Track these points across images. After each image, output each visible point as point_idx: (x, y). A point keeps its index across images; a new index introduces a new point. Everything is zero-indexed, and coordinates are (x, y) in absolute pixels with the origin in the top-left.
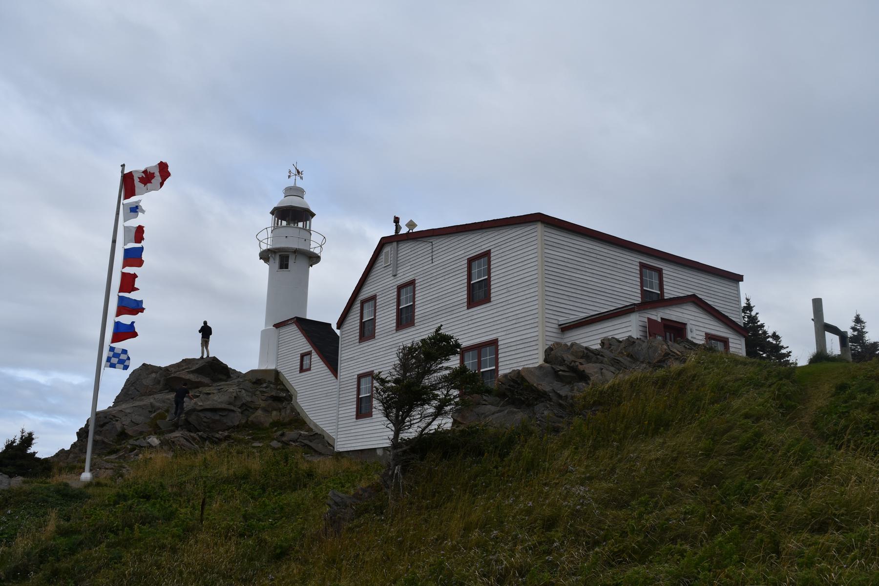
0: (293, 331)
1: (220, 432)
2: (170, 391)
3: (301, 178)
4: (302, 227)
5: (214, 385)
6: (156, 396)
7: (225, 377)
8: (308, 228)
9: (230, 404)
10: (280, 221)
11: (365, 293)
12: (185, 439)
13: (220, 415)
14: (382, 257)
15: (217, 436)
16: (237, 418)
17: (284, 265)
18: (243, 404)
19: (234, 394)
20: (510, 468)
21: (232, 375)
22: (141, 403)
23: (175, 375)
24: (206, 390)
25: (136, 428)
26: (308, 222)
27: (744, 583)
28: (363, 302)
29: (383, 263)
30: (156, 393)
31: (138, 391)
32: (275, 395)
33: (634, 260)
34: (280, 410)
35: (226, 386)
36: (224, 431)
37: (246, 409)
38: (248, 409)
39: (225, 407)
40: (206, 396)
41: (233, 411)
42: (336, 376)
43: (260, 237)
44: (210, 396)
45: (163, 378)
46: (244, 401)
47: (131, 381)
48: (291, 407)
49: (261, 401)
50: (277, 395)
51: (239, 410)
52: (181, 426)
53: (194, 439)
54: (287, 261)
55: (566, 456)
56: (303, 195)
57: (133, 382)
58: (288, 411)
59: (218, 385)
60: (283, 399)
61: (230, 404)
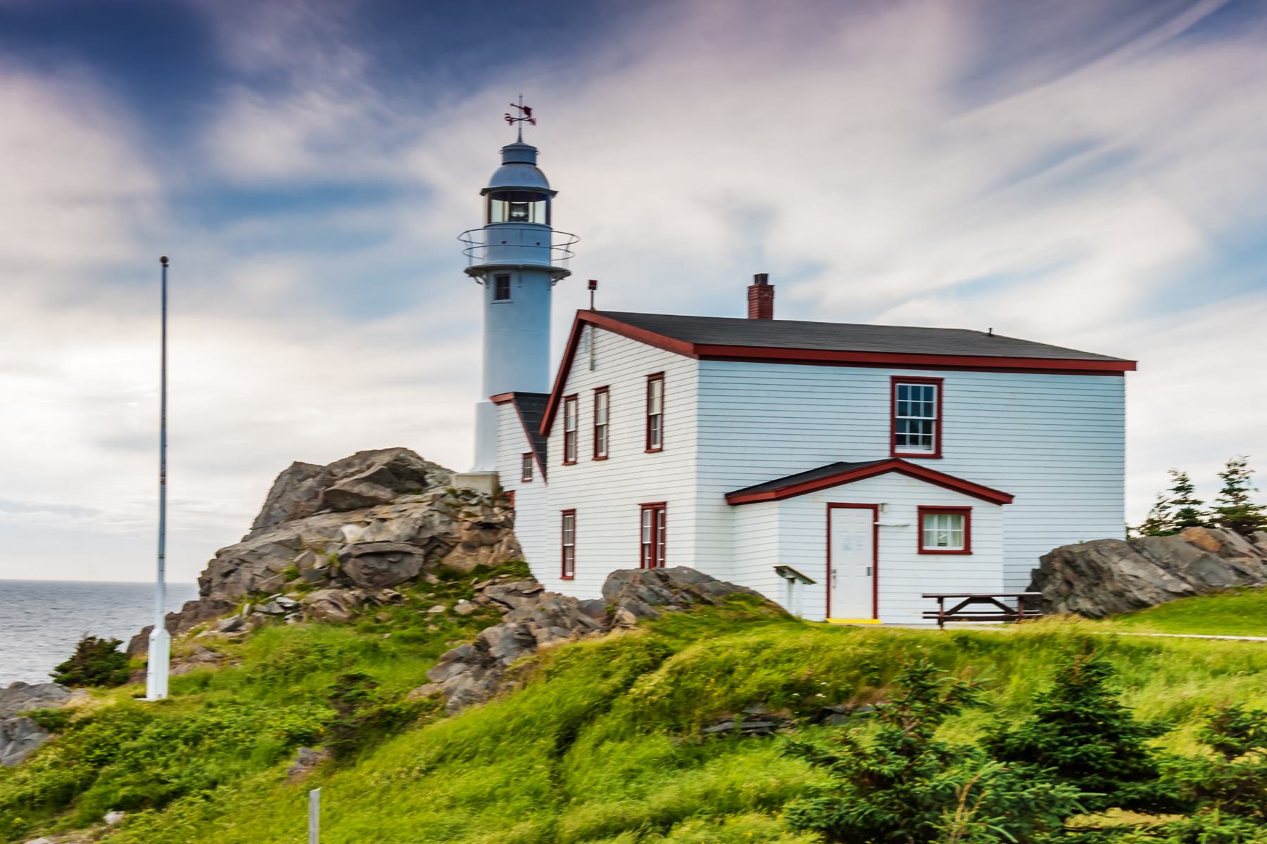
1: (386, 591)
5: (397, 500)
7: (415, 486)
11: (568, 392)
13: (390, 562)
15: (380, 597)
18: (433, 539)
19: (420, 523)
21: (429, 481)
24: (381, 511)
25: (272, 578)
27: (752, 843)
30: (310, 514)
32: (484, 521)
33: (881, 379)
36: (391, 586)
37: (438, 546)
38: (442, 545)
40: (379, 524)
41: (409, 554)
44: (386, 523)
46: (435, 533)
51: (421, 551)
53: (346, 602)
54: (507, 284)
55: (551, 721)
56: (534, 158)
57: (278, 495)
58: (503, 548)
59: (404, 501)
60: (498, 526)
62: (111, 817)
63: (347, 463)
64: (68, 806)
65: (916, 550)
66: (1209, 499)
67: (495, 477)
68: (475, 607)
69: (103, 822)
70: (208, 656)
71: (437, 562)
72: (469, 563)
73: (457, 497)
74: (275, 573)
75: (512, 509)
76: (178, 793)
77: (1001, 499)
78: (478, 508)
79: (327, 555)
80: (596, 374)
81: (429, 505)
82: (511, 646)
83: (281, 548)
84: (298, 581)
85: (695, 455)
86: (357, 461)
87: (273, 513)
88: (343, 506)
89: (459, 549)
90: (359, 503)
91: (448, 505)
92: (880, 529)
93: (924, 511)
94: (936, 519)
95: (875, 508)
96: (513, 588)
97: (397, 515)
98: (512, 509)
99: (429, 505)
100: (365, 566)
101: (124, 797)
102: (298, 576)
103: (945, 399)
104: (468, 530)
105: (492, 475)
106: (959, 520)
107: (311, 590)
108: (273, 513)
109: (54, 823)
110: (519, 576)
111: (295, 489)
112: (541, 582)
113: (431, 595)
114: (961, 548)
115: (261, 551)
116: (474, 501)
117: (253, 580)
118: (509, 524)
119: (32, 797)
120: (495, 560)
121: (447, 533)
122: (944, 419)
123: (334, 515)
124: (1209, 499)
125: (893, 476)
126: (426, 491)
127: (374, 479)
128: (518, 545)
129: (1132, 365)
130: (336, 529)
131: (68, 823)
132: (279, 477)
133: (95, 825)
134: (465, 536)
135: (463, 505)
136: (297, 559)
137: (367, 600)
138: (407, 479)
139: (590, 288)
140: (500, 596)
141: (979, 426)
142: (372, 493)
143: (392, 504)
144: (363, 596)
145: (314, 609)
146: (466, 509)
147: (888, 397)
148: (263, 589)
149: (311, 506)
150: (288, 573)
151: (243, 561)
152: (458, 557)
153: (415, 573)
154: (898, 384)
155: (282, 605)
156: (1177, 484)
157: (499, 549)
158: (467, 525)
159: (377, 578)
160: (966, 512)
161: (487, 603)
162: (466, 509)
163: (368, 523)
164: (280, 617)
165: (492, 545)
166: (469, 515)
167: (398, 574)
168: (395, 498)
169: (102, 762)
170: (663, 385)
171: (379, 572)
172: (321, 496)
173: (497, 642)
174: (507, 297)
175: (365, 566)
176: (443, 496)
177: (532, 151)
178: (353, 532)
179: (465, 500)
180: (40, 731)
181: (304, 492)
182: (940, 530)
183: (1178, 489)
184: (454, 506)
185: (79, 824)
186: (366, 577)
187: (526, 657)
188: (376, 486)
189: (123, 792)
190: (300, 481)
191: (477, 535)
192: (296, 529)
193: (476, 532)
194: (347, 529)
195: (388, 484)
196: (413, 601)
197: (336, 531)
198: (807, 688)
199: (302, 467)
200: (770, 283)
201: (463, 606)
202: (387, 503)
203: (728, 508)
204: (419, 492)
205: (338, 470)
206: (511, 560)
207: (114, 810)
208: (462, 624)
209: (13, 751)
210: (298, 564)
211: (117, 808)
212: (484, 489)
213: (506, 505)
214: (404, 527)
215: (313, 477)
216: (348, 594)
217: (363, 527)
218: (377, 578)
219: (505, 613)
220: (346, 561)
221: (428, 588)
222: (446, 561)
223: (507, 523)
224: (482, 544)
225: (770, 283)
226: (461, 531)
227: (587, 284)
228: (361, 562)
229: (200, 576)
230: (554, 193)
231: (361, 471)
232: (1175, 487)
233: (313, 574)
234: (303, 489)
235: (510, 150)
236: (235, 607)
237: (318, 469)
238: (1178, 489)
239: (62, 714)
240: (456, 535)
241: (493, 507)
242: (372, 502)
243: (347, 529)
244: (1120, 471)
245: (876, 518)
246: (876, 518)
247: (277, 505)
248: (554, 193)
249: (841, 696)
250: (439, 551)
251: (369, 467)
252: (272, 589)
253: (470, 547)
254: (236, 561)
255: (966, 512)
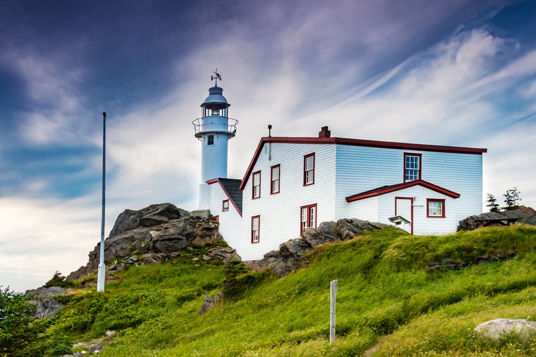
0: (217, 187)
1: (174, 253)
2: (143, 227)
3: (220, 79)
4: (221, 115)
5: (170, 221)
6: (135, 230)
7: (176, 216)
8: (226, 116)
9: (180, 234)
10: (207, 110)
11: (254, 170)
12: (153, 258)
13: (174, 242)
14: (264, 149)
15: (172, 255)
16: (184, 243)
17: (211, 142)
18: (188, 234)
19: (182, 228)
20: (57, 320)
21: (181, 214)
22: (127, 236)
23: (146, 217)
24: (165, 225)
26: (226, 109)
28: (254, 174)
29: (264, 153)
30: (134, 228)
31: (123, 227)
33: (401, 153)
34: (210, 236)
35: (177, 223)
36: (176, 251)
37: (190, 237)
38: (191, 236)
39: (177, 237)
40: (165, 230)
41: (181, 239)
42: (242, 217)
43: (196, 123)
44: (168, 229)
45: (139, 219)
46: (189, 232)
47: (119, 221)
48: (217, 234)
49: (199, 231)
50: (209, 227)
51: (185, 238)
52: (151, 250)
53: (159, 258)
54: (213, 139)
58: (215, 237)
59: (173, 221)
60: (212, 229)
61: (180, 234)
62: (109, 333)
63: (147, 209)
64: (85, 331)
65: (426, 216)
66: (502, 205)
67: (209, 211)
68: (210, 258)
69: (105, 335)
70: (112, 277)
71: (190, 243)
72: (203, 243)
73: (194, 219)
74: (125, 249)
75: (218, 223)
76: (139, 322)
77: (455, 196)
78: (204, 223)
79: (145, 242)
80: (271, 161)
81: (184, 222)
82: (299, 248)
83: (126, 240)
84: (135, 252)
85: (335, 182)
86: (151, 208)
87: (119, 229)
88: (148, 224)
89: (198, 237)
90: (155, 223)
91: (191, 222)
92: (414, 207)
93: (429, 200)
94: (432, 203)
95: (412, 199)
96: (224, 250)
97: (171, 226)
98: (217, 223)
99: (184, 222)
100: (165, 244)
101: (115, 324)
102: (136, 249)
103: (422, 162)
104: (201, 231)
105: (208, 211)
106: (436, 204)
107: (142, 255)
108: (119, 229)
109: (83, 337)
110: (224, 246)
111: (127, 219)
112: (233, 248)
113: (191, 254)
114: (441, 215)
115: (117, 242)
116: (201, 220)
117: (116, 252)
118: (217, 228)
119: (70, 327)
120: (213, 241)
121: (193, 232)
122: (422, 169)
123: (145, 228)
124: (502, 205)
125: (418, 186)
126: (181, 218)
127: (160, 214)
128: (221, 236)
129: (485, 150)
130: (147, 233)
131: (90, 336)
132: (120, 215)
133: (102, 336)
134: (200, 233)
135: (197, 222)
136: (133, 244)
137: (167, 256)
138: (173, 214)
139: (269, 128)
140: (219, 253)
141: (434, 172)
142: (160, 219)
143: (168, 223)
144: (165, 255)
145: (147, 260)
146: (199, 223)
147: (403, 161)
148: (121, 255)
149: (134, 225)
150: (131, 249)
151: (111, 245)
152: (198, 241)
153: (184, 246)
154: (406, 156)
155: (132, 260)
156: (489, 199)
157: (214, 237)
158: (200, 229)
159: (170, 249)
160: (443, 201)
161: (214, 256)
162: (199, 223)
163: (160, 230)
164: (132, 264)
165: (210, 236)
166: (200, 225)
167: (177, 247)
168: (169, 220)
169: (95, 312)
170: (314, 158)
171: (170, 246)
172: (138, 221)
173: (291, 247)
174: (213, 143)
175: (165, 244)
176: (188, 219)
177: (221, 90)
178: (154, 233)
179: (197, 220)
180: (59, 304)
181: (131, 220)
182: (434, 207)
183: (490, 201)
184: (194, 223)
185: (95, 336)
186: (165, 248)
187: (308, 252)
188: (162, 216)
189: (113, 323)
190: (129, 216)
191: (205, 232)
192: (129, 234)
193: (204, 231)
194: (151, 232)
195: (166, 216)
196: (185, 256)
197: (147, 233)
198: (469, 250)
199: (129, 211)
200: (329, 130)
201: (205, 257)
202: (166, 222)
203: (347, 203)
204: (178, 218)
205: (144, 212)
206: (219, 241)
207: (109, 330)
208: (208, 264)
209: (49, 312)
210: (135, 245)
211: (111, 329)
212: (205, 216)
213: (214, 221)
214: (176, 230)
215: (134, 215)
216: (159, 255)
217: (158, 231)
218: (170, 249)
219: (223, 259)
220: (156, 243)
221: (190, 252)
222: (193, 242)
223: (215, 228)
224: (206, 236)
225: (329, 130)
226: (198, 231)
227: (268, 127)
228: (163, 243)
229: (89, 253)
230: (229, 105)
231: (154, 212)
232: (489, 200)
233: (141, 248)
234: (130, 219)
235: (213, 89)
236: (110, 263)
237: (135, 212)
238: (490, 201)
239: (69, 297)
240: (196, 233)
241: (209, 222)
242: (161, 222)
243: (151, 232)
244: (481, 191)
245: (412, 203)
246: (412, 203)
247: (120, 226)
248: (229, 105)
249: (483, 252)
250: (190, 239)
251: (157, 210)
252: (124, 255)
253: (202, 237)
254: (109, 245)
255: (443, 201)
